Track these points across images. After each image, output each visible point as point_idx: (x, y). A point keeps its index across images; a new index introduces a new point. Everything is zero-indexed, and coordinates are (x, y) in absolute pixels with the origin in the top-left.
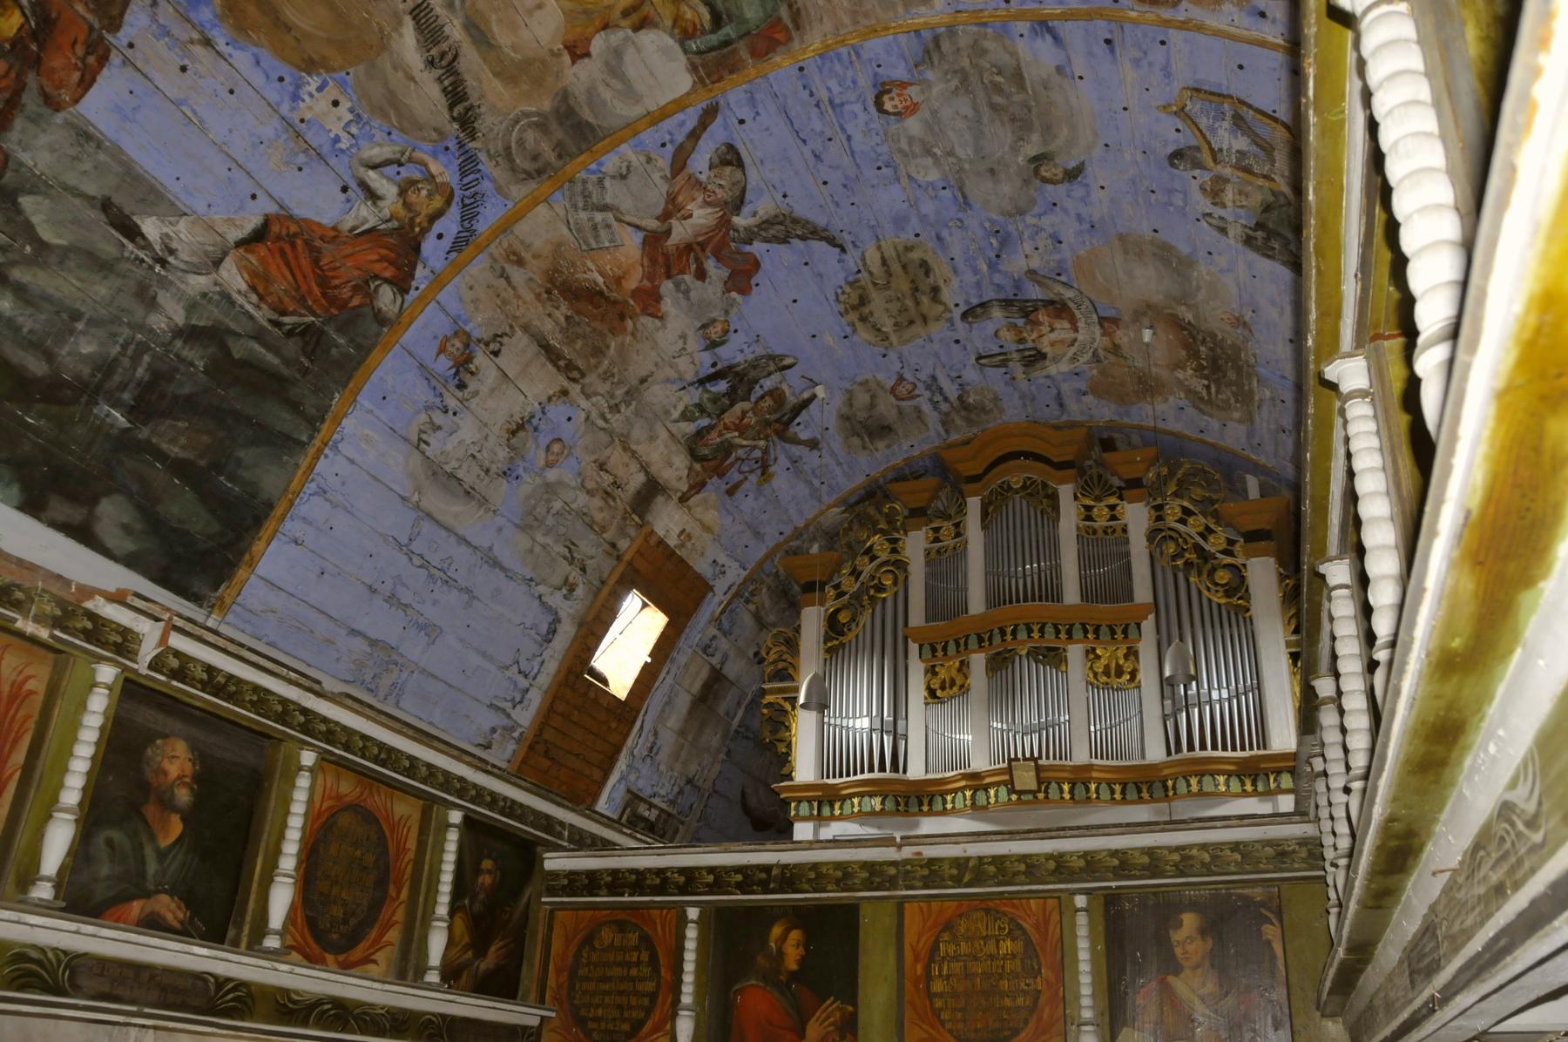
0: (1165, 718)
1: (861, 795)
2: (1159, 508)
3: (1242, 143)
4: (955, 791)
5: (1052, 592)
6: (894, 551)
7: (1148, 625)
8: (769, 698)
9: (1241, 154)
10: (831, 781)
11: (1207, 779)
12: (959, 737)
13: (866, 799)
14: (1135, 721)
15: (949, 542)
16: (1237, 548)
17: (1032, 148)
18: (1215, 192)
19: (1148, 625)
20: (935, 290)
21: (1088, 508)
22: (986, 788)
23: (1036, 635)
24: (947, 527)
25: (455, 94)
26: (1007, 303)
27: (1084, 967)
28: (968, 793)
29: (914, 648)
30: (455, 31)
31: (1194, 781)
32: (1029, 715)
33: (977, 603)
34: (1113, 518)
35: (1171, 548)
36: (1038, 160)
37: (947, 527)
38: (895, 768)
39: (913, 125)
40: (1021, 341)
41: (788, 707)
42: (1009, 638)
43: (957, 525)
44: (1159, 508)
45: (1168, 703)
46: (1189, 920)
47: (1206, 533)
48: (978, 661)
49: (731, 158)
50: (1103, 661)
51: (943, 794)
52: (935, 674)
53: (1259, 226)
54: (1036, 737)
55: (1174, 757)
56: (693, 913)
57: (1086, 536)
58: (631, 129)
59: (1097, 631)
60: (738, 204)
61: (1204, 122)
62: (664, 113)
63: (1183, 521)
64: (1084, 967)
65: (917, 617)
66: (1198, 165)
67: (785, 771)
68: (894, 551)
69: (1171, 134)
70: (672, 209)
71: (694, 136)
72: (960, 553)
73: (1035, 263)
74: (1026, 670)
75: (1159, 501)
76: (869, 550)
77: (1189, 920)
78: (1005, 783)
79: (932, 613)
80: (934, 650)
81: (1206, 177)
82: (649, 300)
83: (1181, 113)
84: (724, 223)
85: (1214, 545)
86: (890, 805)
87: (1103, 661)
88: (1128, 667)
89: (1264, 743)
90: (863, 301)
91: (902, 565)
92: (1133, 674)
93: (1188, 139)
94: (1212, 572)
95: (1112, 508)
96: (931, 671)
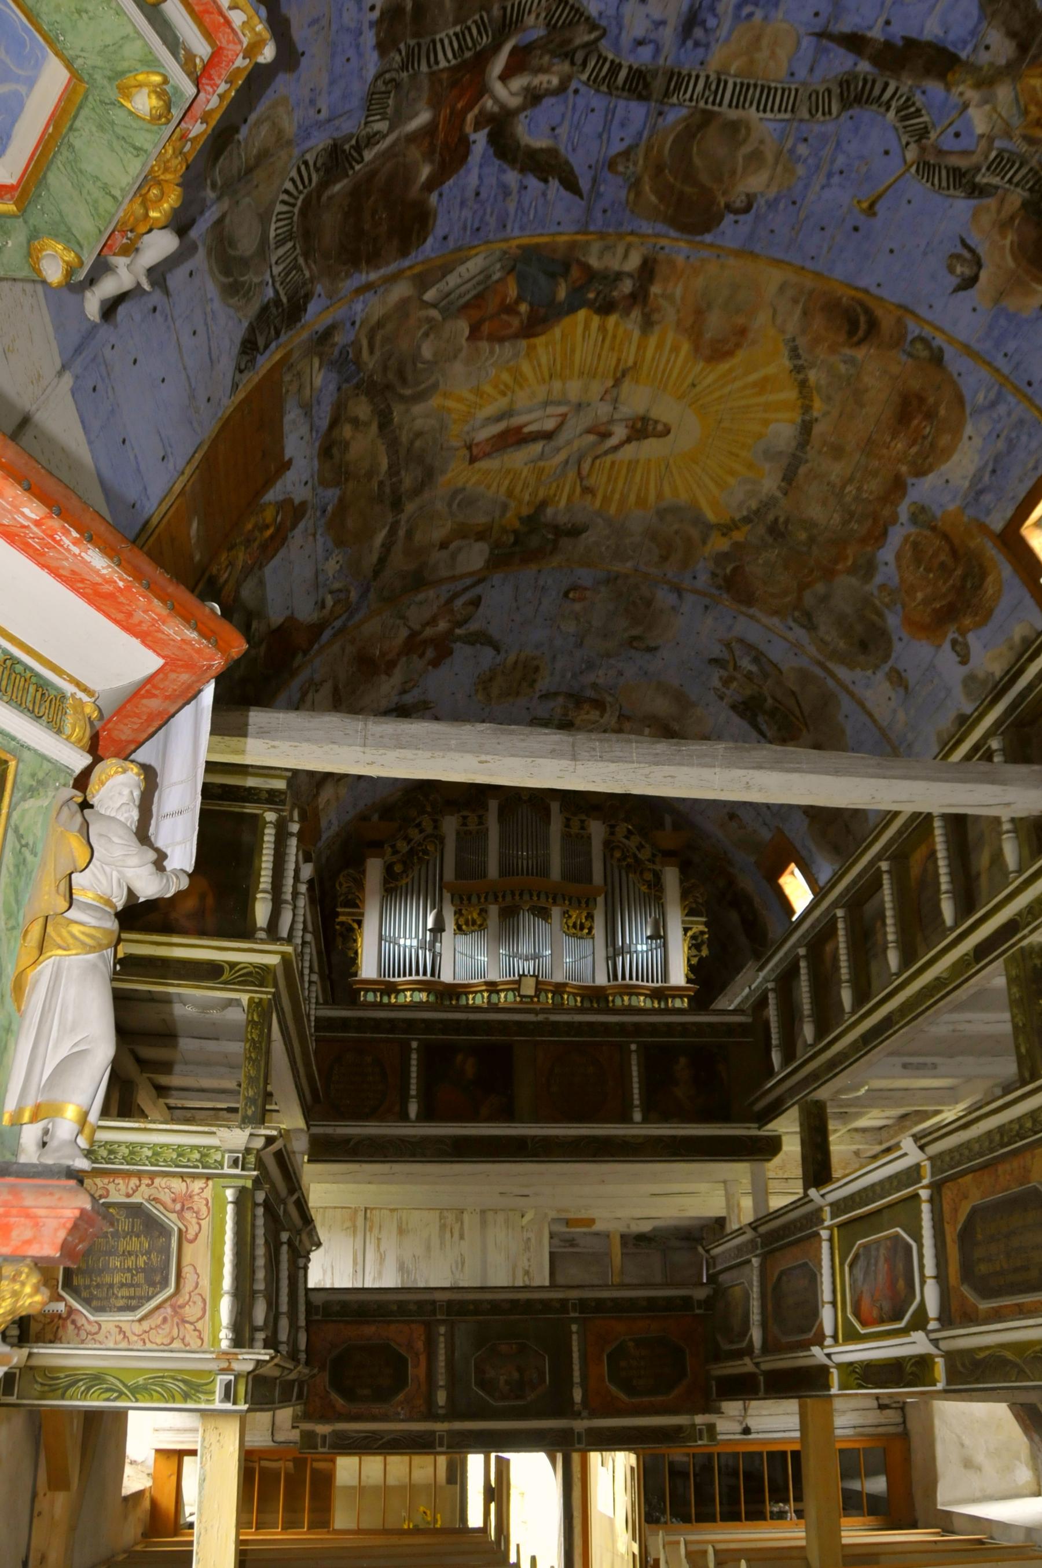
0: (608, 958)
1: (413, 990)
2: (612, 827)
3: (754, 668)
4: (476, 992)
5: (544, 871)
6: (436, 827)
7: (600, 900)
8: (342, 919)
9: (750, 672)
10: (392, 979)
11: (634, 998)
12: (469, 961)
13: (416, 993)
14: (590, 959)
15: (472, 827)
16: (658, 860)
17: (635, 632)
18: (726, 682)
19: (600, 900)
20: (535, 681)
21: (568, 820)
22: (498, 992)
23: (535, 898)
24: (473, 818)
25: (382, 561)
26: (569, 695)
27: (635, 1079)
28: (486, 995)
29: (447, 896)
30: (401, 533)
31: (626, 998)
32: (525, 948)
33: (493, 870)
34: (583, 828)
35: (618, 854)
36: (635, 638)
37: (473, 818)
38: (433, 974)
39: (577, 607)
40: (566, 715)
41: (356, 926)
42: (517, 897)
43: (480, 817)
44: (612, 827)
45: (611, 949)
46: (683, 1061)
47: (640, 847)
48: (494, 910)
49: (476, 602)
50: (573, 919)
51: (467, 994)
52: (461, 914)
53: (744, 703)
54: (532, 963)
55: (612, 983)
56: (414, 1045)
57: (566, 837)
58: (441, 581)
59: (570, 900)
60: (460, 624)
61: (737, 653)
62: (462, 577)
63: (626, 837)
64: (635, 1079)
65: (449, 875)
66: (724, 668)
67: (353, 969)
68: (436, 827)
69: (717, 651)
70: (433, 621)
71: (466, 589)
72: (484, 834)
73: (601, 681)
74: (526, 919)
75: (613, 822)
76: (419, 825)
77: (683, 1061)
78: (513, 990)
79: (460, 874)
80: (461, 899)
81: (725, 674)
82: (391, 665)
83: (728, 645)
84: (450, 632)
85: (644, 855)
86: (432, 998)
87: (573, 919)
88: (588, 924)
89: (665, 976)
90: (491, 679)
91: (442, 840)
92: (590, 929)
93: (726, 655)
94: (641, 873)
95: (582, 821)
96: (458, 913)
